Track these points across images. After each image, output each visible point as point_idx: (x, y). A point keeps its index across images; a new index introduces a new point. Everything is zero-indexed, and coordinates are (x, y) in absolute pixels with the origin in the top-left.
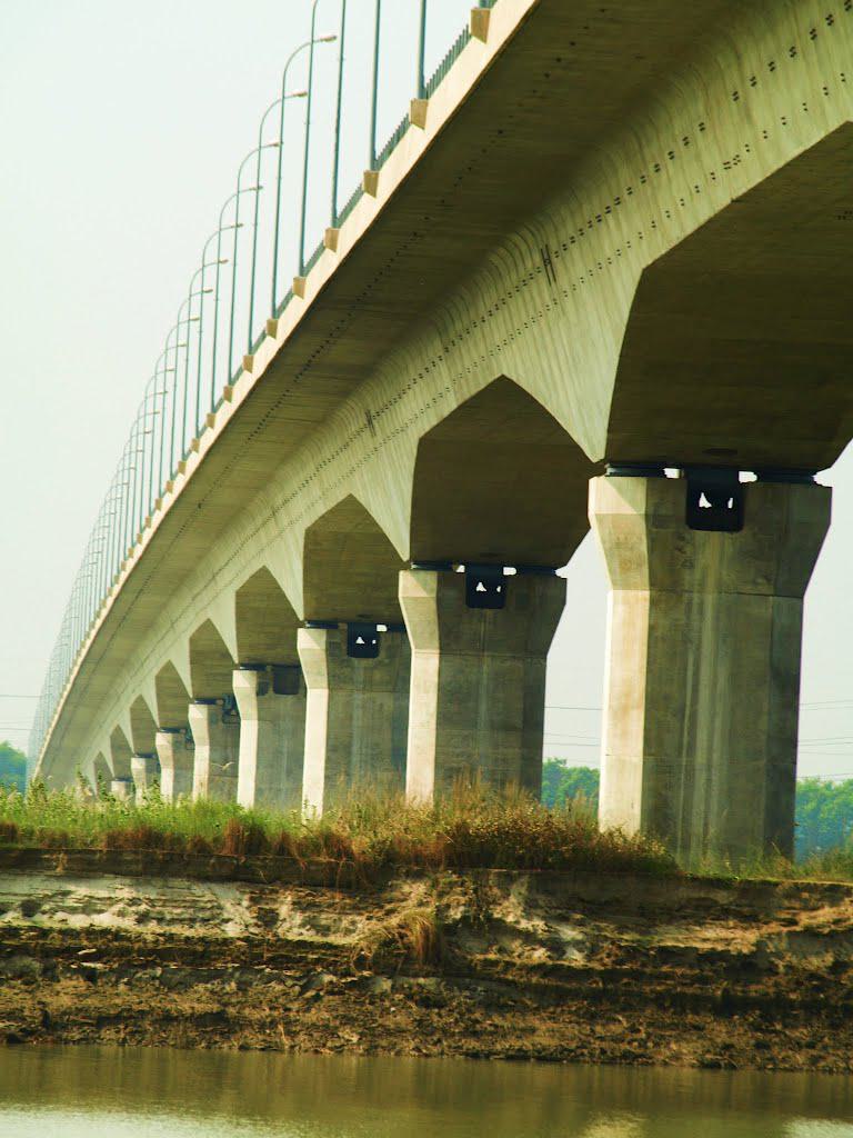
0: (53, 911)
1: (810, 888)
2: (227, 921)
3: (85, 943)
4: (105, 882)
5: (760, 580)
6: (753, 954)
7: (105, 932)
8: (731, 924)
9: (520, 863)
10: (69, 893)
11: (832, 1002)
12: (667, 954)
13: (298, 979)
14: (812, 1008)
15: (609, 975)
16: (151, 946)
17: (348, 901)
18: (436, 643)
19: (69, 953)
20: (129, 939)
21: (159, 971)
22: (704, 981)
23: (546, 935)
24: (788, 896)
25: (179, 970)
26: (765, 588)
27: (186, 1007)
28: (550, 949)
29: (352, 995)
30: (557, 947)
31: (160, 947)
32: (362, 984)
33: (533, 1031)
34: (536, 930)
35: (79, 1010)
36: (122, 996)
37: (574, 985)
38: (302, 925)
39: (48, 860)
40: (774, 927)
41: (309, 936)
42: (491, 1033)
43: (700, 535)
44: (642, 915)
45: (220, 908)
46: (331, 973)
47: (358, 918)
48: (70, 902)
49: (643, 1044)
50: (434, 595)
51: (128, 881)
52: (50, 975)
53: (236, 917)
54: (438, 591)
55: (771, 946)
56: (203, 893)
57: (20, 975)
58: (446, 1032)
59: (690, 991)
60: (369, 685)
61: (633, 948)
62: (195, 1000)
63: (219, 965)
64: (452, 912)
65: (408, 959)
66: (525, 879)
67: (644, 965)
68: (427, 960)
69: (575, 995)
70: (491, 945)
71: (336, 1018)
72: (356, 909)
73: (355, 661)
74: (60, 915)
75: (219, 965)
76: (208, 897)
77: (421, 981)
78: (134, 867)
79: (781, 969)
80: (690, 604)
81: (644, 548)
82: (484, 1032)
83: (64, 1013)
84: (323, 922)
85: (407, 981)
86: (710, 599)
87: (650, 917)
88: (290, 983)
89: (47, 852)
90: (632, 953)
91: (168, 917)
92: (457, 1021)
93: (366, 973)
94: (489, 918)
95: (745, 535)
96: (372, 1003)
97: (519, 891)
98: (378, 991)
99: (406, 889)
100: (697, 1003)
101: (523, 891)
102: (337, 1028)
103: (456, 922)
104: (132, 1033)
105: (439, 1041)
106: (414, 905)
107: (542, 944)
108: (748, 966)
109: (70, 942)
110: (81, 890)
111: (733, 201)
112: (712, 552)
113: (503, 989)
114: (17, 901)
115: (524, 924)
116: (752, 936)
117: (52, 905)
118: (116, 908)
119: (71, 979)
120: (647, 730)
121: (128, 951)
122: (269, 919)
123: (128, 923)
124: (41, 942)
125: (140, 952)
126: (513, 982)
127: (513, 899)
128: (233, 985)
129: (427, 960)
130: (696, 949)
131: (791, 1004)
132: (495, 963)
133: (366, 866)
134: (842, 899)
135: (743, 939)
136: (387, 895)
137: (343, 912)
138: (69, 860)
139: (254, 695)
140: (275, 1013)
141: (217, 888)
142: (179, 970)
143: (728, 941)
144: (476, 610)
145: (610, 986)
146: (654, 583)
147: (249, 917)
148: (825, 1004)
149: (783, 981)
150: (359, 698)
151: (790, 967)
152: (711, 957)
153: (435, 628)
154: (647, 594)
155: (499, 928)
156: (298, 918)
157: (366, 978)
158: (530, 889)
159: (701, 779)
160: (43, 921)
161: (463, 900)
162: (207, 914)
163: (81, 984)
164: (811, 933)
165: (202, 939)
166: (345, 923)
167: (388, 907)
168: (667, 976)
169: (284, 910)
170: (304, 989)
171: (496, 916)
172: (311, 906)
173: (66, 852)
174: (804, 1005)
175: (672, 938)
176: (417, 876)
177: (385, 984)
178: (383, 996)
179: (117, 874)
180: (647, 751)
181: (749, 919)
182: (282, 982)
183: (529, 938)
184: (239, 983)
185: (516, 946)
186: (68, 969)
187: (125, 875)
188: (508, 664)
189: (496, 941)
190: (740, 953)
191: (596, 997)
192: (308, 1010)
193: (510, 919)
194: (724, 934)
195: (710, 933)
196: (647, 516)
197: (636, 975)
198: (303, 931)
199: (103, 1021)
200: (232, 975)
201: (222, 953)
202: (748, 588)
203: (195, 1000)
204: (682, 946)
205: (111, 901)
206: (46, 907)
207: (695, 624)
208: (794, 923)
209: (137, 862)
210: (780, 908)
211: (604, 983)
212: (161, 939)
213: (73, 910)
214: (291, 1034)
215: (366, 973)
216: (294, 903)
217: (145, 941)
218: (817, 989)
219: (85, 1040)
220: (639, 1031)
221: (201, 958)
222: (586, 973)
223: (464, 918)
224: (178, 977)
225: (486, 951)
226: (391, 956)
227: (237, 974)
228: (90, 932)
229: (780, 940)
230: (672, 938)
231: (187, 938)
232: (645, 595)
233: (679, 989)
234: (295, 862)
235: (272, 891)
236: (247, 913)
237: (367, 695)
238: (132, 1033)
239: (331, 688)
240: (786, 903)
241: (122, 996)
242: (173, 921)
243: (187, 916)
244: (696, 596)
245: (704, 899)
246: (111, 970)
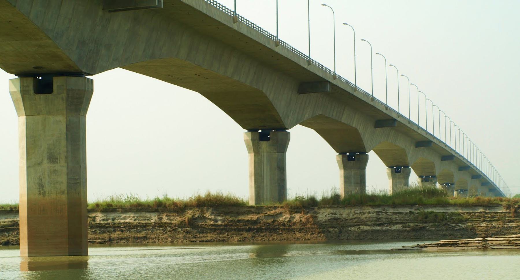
0: (118, 219)
1: (270, 207)
2: (152, 219)
3: (122, 225)
4: (129, 214)
5: (274, 150)
6: (256, 220)
7: (127, 223)
8: (254, 214)
9: (211, 206)
10: (122, 216)
11: (271, 228)
12: (239, 221)
13: (163, 229)
14: (267, 229)
15: (225, 226)
16: (135, 225)
17: (176, 215)
18: (343, 168)
19: (118, 227)
20: (131, 224)
21: (136, 229)
22: (245, 225)
23: (214, 219)
24: (266, 209)
25: (140, 229)
26: (276, 152)
27: (141, 236)
28: (215, 221)
29: (173, 232)
30: (216, 221)
31: (137, 225)
32: (175, 230)
33: (207, 237)
34: (212, 218)
35: (117, 237)
36: (128, 234)
37: (218, 228)
38: (167, 220)
39: (118, 210)
40: (262, 215)
41: (168, 221)
42: (199, 238)
43: (262, 142)
44: (237, 214)
45: (151, 217)
46: (169, 228)
47: (178, 218)
48: (121, 218)
49: (228, 238)
50: (341, 159)
51: (133, 213)
52: (114, 231)
53: (154, 218)
54: (342, 158)
55: (261, 218)
56: (148, 215)
57: (108, 232)
58: (189, 238)
59: (241, 227)
60: (399, 178)
61: (231, 220)
62: (142, 234)
63: (148, 228)
64: (196, 216)
65: (185, 225)
66: (211, 209)
67: (233, 223)
68: (189, 225)
69: (218, 229)
70: (203, 221)
71: (168, 236)
72: (178, 216)
73: (397, 174)
74: (119, 220)
75: (148, 228)
76: (149, 215)
77: (187, 228)
78: (134, 211)
79: (262, 222)
80: (261, 155)
81: (252, 146)
82: (197, 237)
83: (114, 238)
84: (171, 219)
85: (184, 229)
86: (265, 154)
87: (238, 214)
88: (161, 230)
89: (118, 209)
90: (231, 221)
91: (140, 219)
92: (192, 236)
93: (176, 228)
94: (203, 216)
95: (270, 141)
96: (176, 233)
97: (210, 210)
98: (178, 231)
99: (188, 212)
100: (243, 230)
101: (211, 211)
102: (168, 238)
103: (196, 217)
104: (127, 241)
105: (187, 239)
106: (189, 214)
107: (213, 220)
108: (255, 222)
109: (120, 225)
110: (124, 215)
111: (93, 75)
112: (264, 145)
113: (204, 229)
114: (111, 218)
115: (210, 217)
116: (257, 217)
117: (118, 218)
118: (130, 218)
119: (118, 232)
120: (255, 180)
121: (130, 226)
122: (160, 219)
123: (132, 221)
124: (113, 225)
125: (133, 226)
126: (206, 228)
127: (209, 213)
128: (150, 231)
129: (189, 225)
130: (245, 220)
131: (263, 229)
132: (203, 224)
133: (180, 208)
134: (277, 209)
135: (254, 217)
136: (184, 213)
137: (175, 217)
138: (122, 210)
139: (421, 182)
140: (157, 236)
141: (151, 214)
142: (140, 229)
143: (252, 218)
144: (350, 161)
145: (225, 227)
146: (254, 152)
147: (157, 219)
148: (269, 228)
149: (262, 224)
150: (398, 181)
151: (264, 222)
152: (248, 221)
153: (342, 165)
154: (253, 154)
155: (204, 218)
156: (166, 218)
157: (176, 229)
158: (212, 211)
159: (265, 188)
160: (116, 221)
161: (198, 213)
162: (148, 218)
163: (120, 232)
164: (269, 215)
165: (145, 223)
166: (175, 219)
167: (184, 215)
168: (237, 225)
169: (164, 217)
170: (164, 231)
171: (205, 216)
172: (169, 216)
173: (121, 208)
174: (265, 229)
175: (240, 218)
176: (191, 209)
177: (180, 229)
178: (179, 231)
179: (131, 212)
180: (255, 184)
181: (258, 213)
182: (160, 230)
183: (210, 219)
184: (152, 231)
185: (208, 221)
186: (118, 230)
187: (133, 212)
188: (356, 171)
189: (205, 220)
190: (254, 220)
191: (222, 230)
192: (164, 235)
193: (207, 216)
194: (252, 217)
195: (249, 217)
196: (251, 139)
197: (231, 225)
198: (167, 221)
199: (122, 239)
200: (150, 229)
201: (149, 226)
202: (272, 152)
203: (142, 234)
204: (242, 219)
205: (129, 217)
206: (117, 219)
207: (262, 159)
208: (266, 214)
209: (135, 210)
210: (264, 211)
211: (224, 227)
212: (137, 223)
213: (122, 219)
214: (158, 240)
215: (176, 228)
216: (166, 216)
217: (134, 224)
218: (268, 226)
219: (117, 243)
220: (228, 235)
221: (144, 227)
222: (221, 225)
223: (198, 217)
224: (140, 231)
225: (202, 223)
226: (182, 225)
227: (152, 229)
228: (124, 223)
229: (263, 217)
230: (240, 218)
231: (143, 223)
232: (253, 154)
233: (239, 227)
234: (167, 208)
235: (162, 214)
236: (157, 218)
237: (399, 180)
238: (127, 241)
239: (392, 179)
240: (266, 210)
241: (128, 234)
242: (141, 220)
243: (144, 219)
244: (262, 154)
245: (249, 210)
246: (126, 230)
